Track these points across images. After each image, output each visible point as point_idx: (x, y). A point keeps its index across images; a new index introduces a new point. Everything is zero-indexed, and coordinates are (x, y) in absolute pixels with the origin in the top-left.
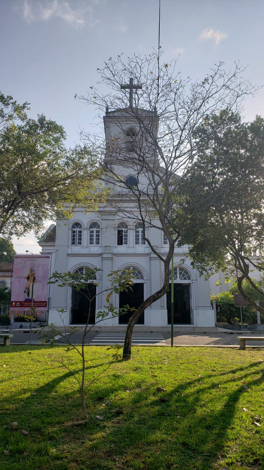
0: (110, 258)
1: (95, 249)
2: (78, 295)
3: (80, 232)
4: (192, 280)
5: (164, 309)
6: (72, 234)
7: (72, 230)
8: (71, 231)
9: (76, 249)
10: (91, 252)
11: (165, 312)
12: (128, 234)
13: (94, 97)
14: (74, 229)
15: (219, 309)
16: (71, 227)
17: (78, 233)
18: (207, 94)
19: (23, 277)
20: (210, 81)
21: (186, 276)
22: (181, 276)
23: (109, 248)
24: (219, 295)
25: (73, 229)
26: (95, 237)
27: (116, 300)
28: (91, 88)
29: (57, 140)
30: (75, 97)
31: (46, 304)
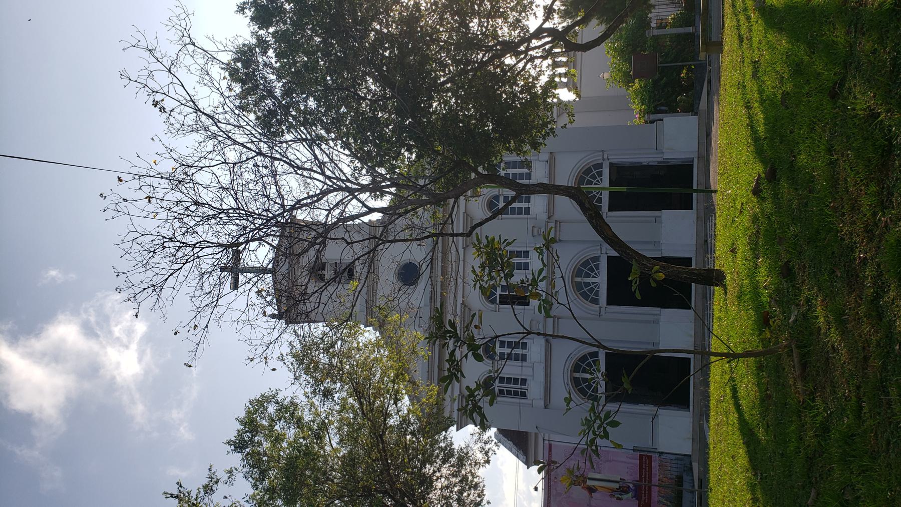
0: (554, 322)
3: (502, 380)
4: (604, 160)
6: (506, 395)
9: (535, 389)
10: (543, 360)
11: (666, 214)
13: (195, 329)
17: (505, 385)
18: (188, 104)
19: (590, 500)
20: (158, 97)
21: (594, 172)
22: (594, 181)
24: (637, 107)
27: (649, 314)
28: (176, 333)
31: (646, 456)
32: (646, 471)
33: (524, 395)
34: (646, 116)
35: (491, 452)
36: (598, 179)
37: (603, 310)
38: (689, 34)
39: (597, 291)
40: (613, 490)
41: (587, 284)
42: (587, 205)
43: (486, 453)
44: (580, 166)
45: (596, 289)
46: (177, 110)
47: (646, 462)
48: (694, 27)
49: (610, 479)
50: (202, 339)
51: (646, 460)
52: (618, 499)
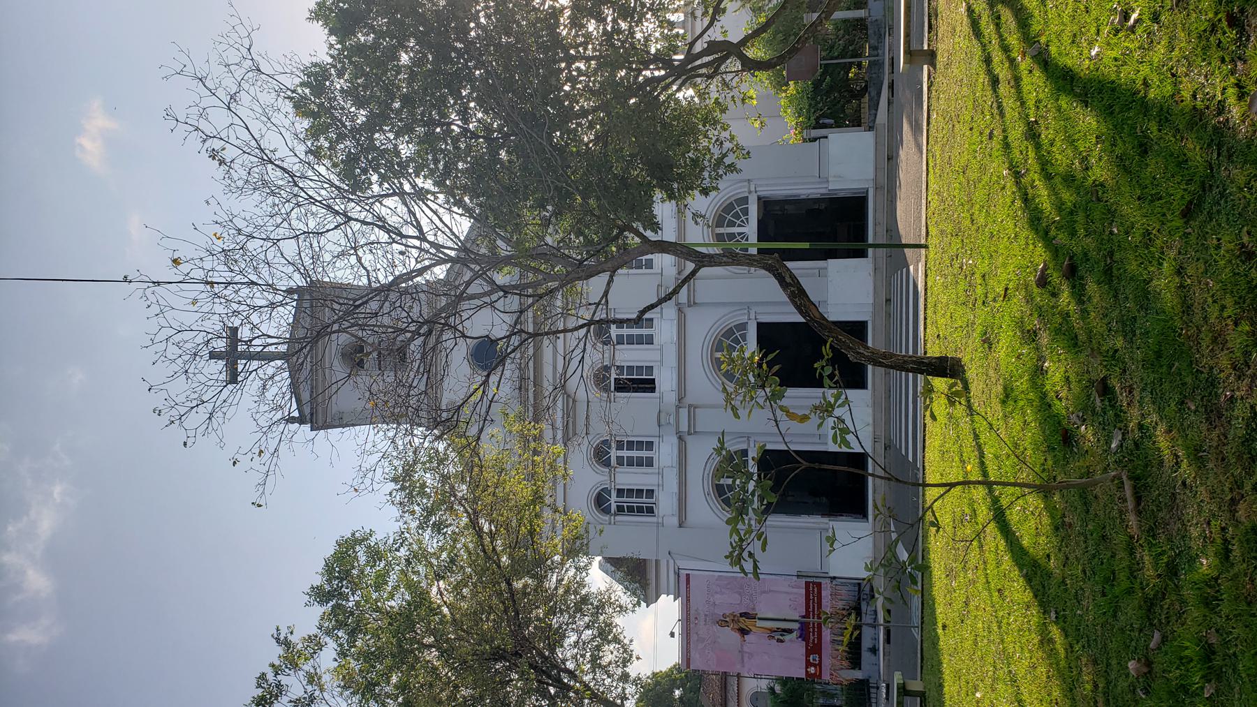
0: (689, 412)
1: (666, 453)
2: (789, 499)
3: (620, 492)
6: (626, 513)
7: (616, 515)
8: (618, 518)
9: (666, 503)
10: (675, 464)
11: (834, 264)
12: (625, 364)
15: (827, 121)
16: (607, 518)
17: (625, 499)
19: (742, 645)
20: (217, 144)
21: (738, 209)
22: (738, 222)
23: (662, 415)
25: (613, 512)
26: (635, 454)
28: (234, 463)
31: (814, 583)
32: (814, 602)
33: (650, 511)
34: (805, 131)
36: (743, 218)
38: (861, 19)
40: (772, 631)
42: (788, 280)
44: (719, 201)
46: (238, 161)
47: (813, 591)
48: (867, 10)
49: (787, 618)
50: (272, 468)
51: (813, 588)
52: (779, 641)
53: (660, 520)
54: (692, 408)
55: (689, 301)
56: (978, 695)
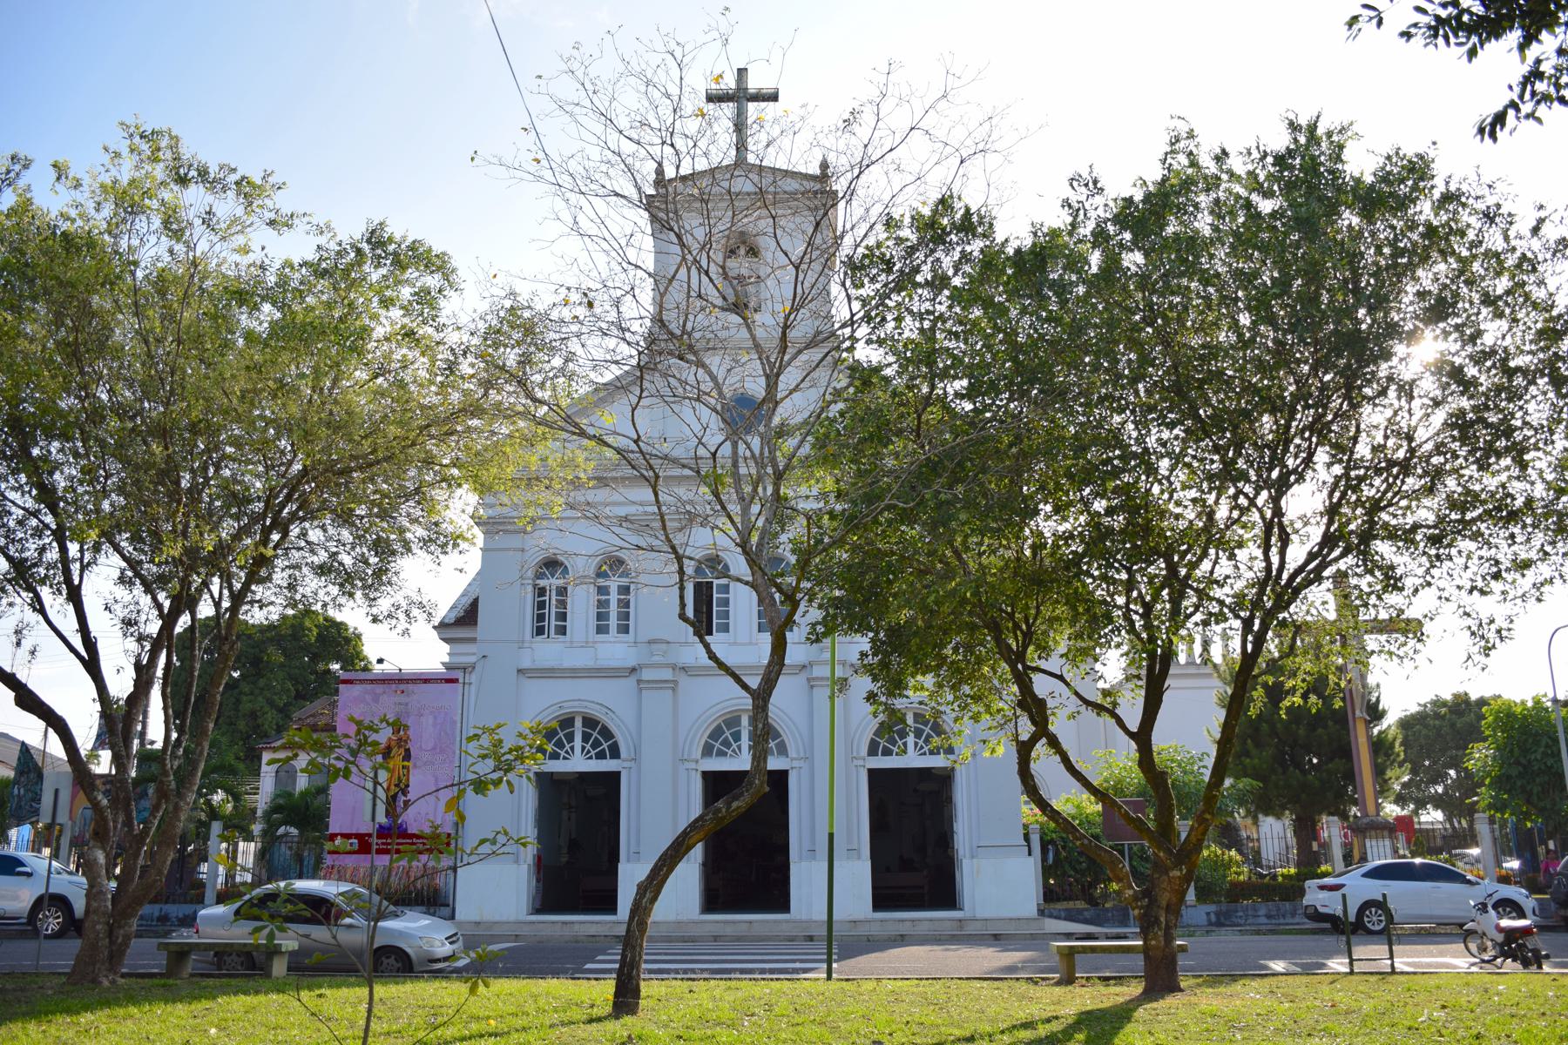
1: (615, 650)
2: (565, 814)
3: (562, 591)
5: (859, 858)
7: (535, 586)
8: (530, 589)
9: (548, 651)
12: (731, 596)
14: (542, 583)
15: (1051, 855)
16: (530, 574)
17: (554, 598)
23: (664, 646)
25: (538, 582)
26: (613, 609)
29: (425, 298)
30: (472, 159)
33: (540, 631)
35: (394, 622)
37: (693, 765)
39: (725, 754)
41: (570, 738)
43: (390, 616)
45: (730, 752)
53: (526, 645)
54: (673, 686)
55: (814, 679)
56: (213, 1031)
